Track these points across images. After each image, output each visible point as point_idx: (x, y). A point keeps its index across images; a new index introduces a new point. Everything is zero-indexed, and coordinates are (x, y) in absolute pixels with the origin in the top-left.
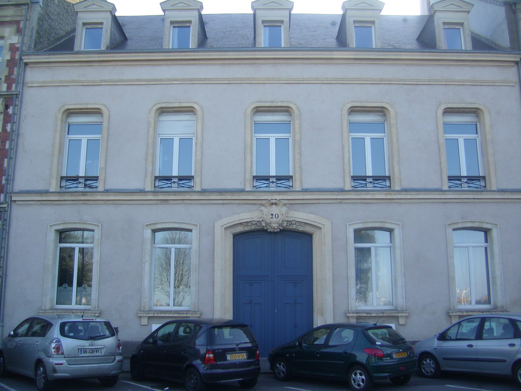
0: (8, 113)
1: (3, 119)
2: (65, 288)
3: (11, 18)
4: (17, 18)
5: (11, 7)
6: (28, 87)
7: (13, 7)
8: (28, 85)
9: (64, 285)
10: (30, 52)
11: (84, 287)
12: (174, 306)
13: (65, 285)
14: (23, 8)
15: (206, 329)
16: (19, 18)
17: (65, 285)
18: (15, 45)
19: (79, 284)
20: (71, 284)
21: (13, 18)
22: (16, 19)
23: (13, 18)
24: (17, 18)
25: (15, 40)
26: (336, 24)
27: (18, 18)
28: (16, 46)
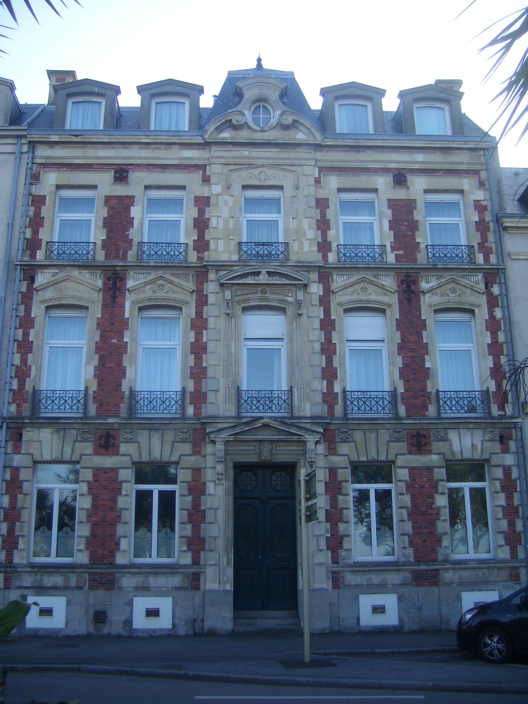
0: (492, 294)
1: (487, 302)
2: (66, 533)
3: (468, 167)
4: (476, 167)
5: (464, 151)
6: (512, 259)
7: (468, 152)
8: (513, 257)
9: (64, 529)
10: (502, 213)
11: (65, 531)
12: (57, 557)
13: (66, 529)
14: (480, 154)
15: (133, 586)
16: (478, 167)
17: (66, 529)
18: (481, 202)
19: (61, 526)
20: (50, 528)
21: (470, 167)
22: (474, 167)
23: (470, 167)
24: (476, 167)
25: (480, 195)
26: (519, 175)
27: (478, 167)
28: (481, 204)
